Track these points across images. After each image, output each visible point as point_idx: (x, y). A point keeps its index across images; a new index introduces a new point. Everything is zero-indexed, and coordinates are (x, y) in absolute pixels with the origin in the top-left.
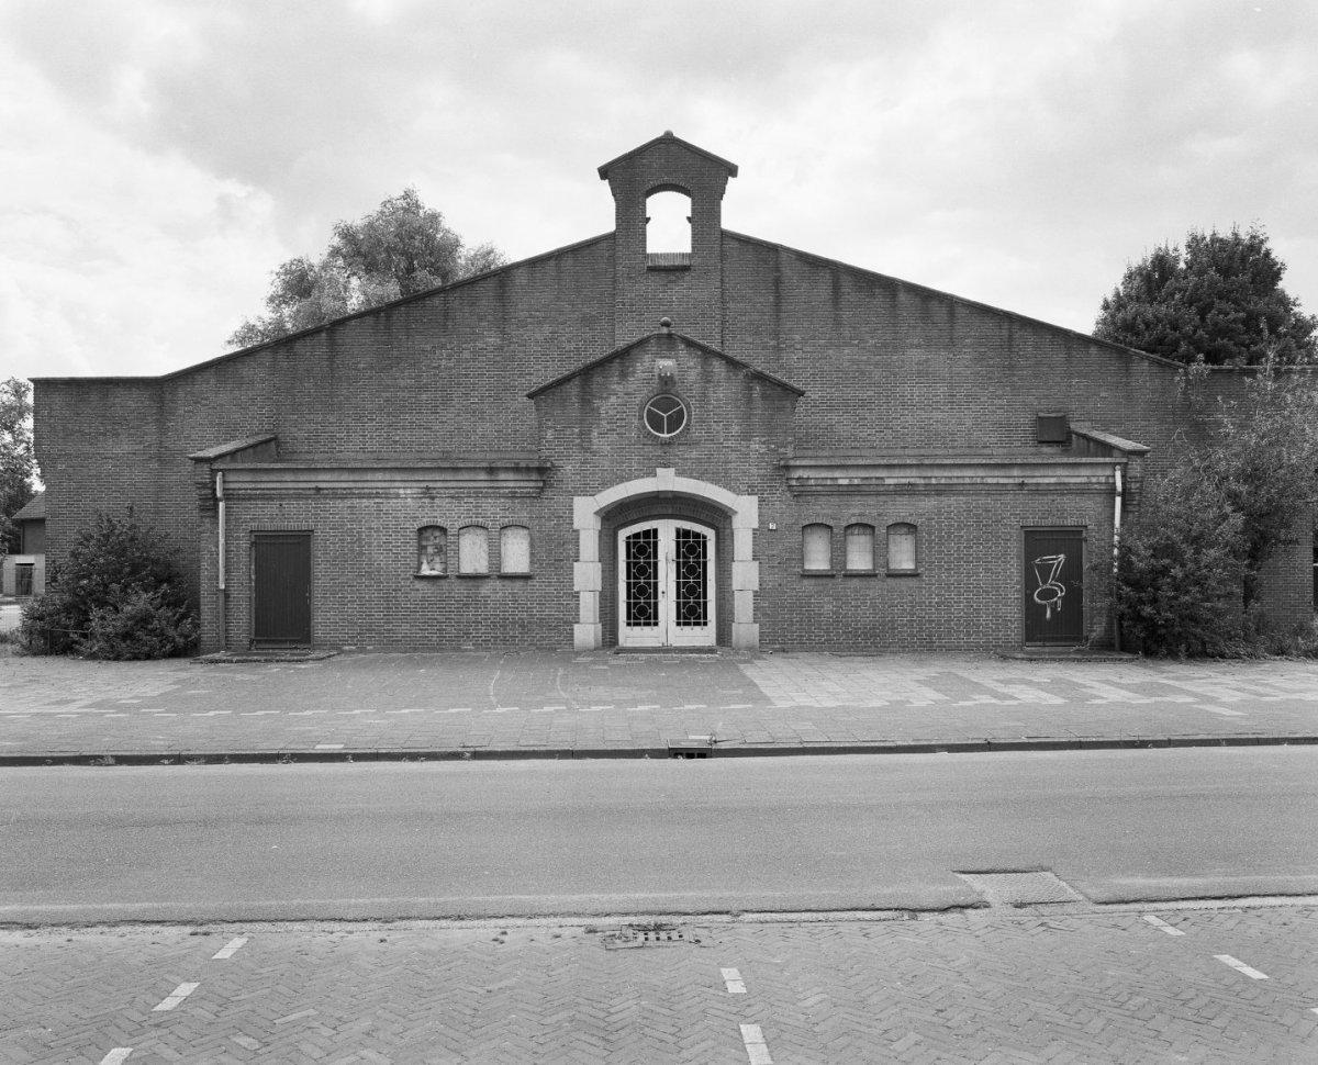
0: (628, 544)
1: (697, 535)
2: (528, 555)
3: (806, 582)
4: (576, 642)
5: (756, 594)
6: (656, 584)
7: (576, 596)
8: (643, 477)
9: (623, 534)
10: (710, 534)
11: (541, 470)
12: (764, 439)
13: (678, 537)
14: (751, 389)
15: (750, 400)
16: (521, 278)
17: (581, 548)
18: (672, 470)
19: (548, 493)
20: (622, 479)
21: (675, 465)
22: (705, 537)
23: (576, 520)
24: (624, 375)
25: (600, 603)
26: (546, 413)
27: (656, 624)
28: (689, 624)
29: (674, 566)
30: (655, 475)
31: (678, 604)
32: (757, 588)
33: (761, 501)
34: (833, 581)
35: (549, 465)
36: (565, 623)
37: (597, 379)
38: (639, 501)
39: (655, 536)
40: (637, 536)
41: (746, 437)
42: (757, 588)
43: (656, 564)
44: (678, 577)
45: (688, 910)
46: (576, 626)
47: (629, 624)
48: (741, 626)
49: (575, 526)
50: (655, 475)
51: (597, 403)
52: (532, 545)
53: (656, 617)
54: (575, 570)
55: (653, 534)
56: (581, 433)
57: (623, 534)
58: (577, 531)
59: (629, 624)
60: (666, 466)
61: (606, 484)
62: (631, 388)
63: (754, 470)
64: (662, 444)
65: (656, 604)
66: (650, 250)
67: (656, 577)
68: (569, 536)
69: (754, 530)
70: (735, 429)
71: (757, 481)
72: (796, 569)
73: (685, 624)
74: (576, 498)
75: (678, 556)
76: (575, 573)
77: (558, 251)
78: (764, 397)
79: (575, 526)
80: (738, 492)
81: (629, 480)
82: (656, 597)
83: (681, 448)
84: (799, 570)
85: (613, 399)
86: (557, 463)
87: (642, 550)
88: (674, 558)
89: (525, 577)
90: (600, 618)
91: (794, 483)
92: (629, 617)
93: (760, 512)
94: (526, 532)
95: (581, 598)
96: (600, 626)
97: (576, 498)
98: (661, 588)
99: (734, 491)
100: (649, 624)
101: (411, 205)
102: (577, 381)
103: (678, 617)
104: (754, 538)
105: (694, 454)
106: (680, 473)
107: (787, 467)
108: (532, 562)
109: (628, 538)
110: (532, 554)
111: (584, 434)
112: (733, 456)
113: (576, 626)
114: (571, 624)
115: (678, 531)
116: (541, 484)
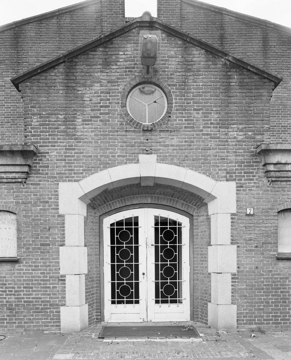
0: (112, 230)
1: (174, 223)
2: (15, 239)
3: (281, 264)
4: (63, 324)
5: (234, 277)
6: (137, 267)
7: (62, 279)
8: (126, 163)
9: (108, 221)
10: (184, 221)
11: (26, 154)
12: (240, 127)
13: (157, 224)
14: (229, 77)
15: (228, 88)
16: (31, 31)
17: (66, 232)
18: (154, 157)
19: (34, 178)
20: (106, 165)
21: (156, 151)
22: (180, 224)
23: (60, 207)
24: (107, 64)
25: (86, 285)
26: (31, 100)
27: (137, 302)
28: (166, 302)
29: (153, 249)
30: (138, 162)
31: (157, 285)
32: (235, 270)
33: (239, 187)
34: (17, 266)
35: (32, 148)
36: (51, 305)
37: (81, 67)
38: (122, 188)
39: (137, 224)
40: (119, 223)
41: (224, 124)
42: (235, 270)
43: (137, 248)
44: (157, 260)
45: (128, 314)
46: (62, 309)
47: (113, 302)
48: (220, 307)
49: (61, 212)
50: (138, 162)
51: (81, 90)
52: (19, 230)
53: (137, 296)
54: (61, 253)
55: (133, 223)
56: (66, 120)
57: (108, 221)
58: (62, 216)
59: (113, 302)
60: (148, 152)
61: (90, 170)
62: (114, 76)
63: (232, 158)
64: (144, 130)
65: (137, 285)
66: (127, 15)
67: (137, 260)
68: (56, 221)
69: (232, 214)
70: (214, 117)
71: (234, 167)
72: (272, 253)
73: (163, 302)
74: (61, 184)
75: (156, 241)
76: (61, 257)
77: (59, 11)
78: (242, 85)
79: (61, 212)
80: (217, 179)
81: (113, 165)
82: (137, 278)
83: (163, 135)
84: (275, 253)
85: (97, 87)
86: (42, 149)
87: (124, 236)
88: (153, 242)
89: (13, 261)
90: (86, 299)
91: (271, 168)
92: (113, 296)
93: (238, 197)
94: (13, 217)
95: (67, 282)
96: (86, 306)
97: (61, 184)
98: (141, 270)
99: (213, 177)
100: (131, 302)
101: (82, 199)
102: (61, 69)
103: (157, 296)
104: (232, 222)
105: (175, 141)
106: (162, 159)
107: (267, 152)
108: (19, 247)
109: (112, 225)
110: (19, 238)
111: (69, 121)
112: (212, 144)
113: (62, 309)
114: (58, 306)
115: (156, 218)
116: (26, 169)
